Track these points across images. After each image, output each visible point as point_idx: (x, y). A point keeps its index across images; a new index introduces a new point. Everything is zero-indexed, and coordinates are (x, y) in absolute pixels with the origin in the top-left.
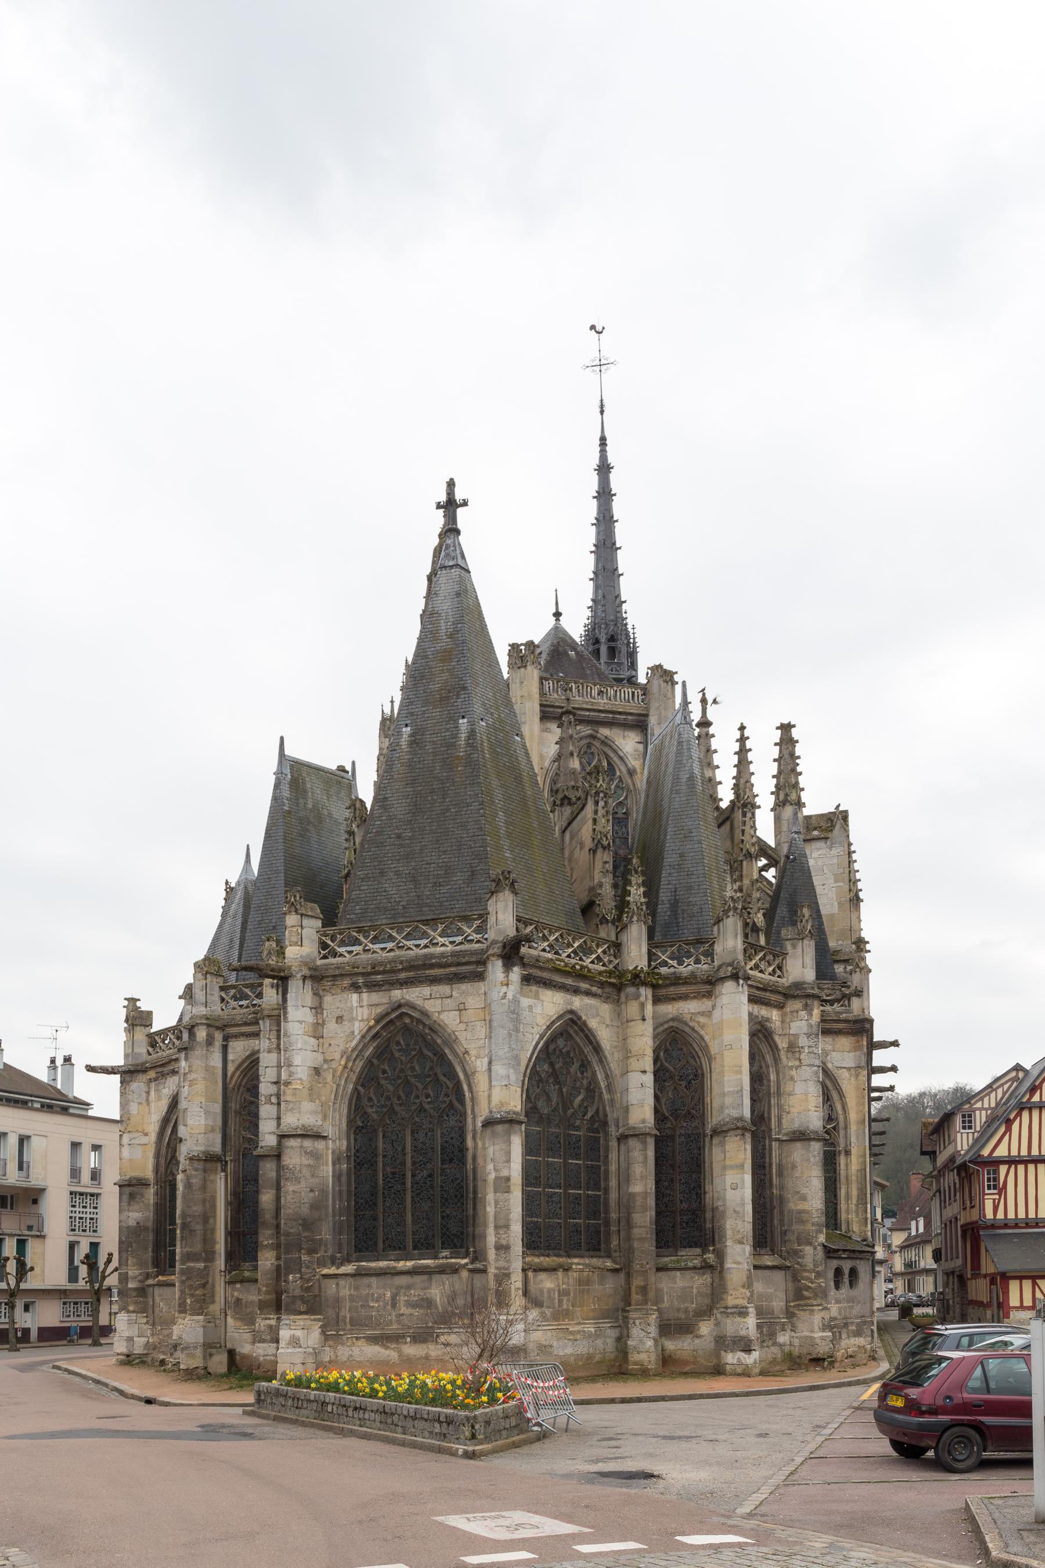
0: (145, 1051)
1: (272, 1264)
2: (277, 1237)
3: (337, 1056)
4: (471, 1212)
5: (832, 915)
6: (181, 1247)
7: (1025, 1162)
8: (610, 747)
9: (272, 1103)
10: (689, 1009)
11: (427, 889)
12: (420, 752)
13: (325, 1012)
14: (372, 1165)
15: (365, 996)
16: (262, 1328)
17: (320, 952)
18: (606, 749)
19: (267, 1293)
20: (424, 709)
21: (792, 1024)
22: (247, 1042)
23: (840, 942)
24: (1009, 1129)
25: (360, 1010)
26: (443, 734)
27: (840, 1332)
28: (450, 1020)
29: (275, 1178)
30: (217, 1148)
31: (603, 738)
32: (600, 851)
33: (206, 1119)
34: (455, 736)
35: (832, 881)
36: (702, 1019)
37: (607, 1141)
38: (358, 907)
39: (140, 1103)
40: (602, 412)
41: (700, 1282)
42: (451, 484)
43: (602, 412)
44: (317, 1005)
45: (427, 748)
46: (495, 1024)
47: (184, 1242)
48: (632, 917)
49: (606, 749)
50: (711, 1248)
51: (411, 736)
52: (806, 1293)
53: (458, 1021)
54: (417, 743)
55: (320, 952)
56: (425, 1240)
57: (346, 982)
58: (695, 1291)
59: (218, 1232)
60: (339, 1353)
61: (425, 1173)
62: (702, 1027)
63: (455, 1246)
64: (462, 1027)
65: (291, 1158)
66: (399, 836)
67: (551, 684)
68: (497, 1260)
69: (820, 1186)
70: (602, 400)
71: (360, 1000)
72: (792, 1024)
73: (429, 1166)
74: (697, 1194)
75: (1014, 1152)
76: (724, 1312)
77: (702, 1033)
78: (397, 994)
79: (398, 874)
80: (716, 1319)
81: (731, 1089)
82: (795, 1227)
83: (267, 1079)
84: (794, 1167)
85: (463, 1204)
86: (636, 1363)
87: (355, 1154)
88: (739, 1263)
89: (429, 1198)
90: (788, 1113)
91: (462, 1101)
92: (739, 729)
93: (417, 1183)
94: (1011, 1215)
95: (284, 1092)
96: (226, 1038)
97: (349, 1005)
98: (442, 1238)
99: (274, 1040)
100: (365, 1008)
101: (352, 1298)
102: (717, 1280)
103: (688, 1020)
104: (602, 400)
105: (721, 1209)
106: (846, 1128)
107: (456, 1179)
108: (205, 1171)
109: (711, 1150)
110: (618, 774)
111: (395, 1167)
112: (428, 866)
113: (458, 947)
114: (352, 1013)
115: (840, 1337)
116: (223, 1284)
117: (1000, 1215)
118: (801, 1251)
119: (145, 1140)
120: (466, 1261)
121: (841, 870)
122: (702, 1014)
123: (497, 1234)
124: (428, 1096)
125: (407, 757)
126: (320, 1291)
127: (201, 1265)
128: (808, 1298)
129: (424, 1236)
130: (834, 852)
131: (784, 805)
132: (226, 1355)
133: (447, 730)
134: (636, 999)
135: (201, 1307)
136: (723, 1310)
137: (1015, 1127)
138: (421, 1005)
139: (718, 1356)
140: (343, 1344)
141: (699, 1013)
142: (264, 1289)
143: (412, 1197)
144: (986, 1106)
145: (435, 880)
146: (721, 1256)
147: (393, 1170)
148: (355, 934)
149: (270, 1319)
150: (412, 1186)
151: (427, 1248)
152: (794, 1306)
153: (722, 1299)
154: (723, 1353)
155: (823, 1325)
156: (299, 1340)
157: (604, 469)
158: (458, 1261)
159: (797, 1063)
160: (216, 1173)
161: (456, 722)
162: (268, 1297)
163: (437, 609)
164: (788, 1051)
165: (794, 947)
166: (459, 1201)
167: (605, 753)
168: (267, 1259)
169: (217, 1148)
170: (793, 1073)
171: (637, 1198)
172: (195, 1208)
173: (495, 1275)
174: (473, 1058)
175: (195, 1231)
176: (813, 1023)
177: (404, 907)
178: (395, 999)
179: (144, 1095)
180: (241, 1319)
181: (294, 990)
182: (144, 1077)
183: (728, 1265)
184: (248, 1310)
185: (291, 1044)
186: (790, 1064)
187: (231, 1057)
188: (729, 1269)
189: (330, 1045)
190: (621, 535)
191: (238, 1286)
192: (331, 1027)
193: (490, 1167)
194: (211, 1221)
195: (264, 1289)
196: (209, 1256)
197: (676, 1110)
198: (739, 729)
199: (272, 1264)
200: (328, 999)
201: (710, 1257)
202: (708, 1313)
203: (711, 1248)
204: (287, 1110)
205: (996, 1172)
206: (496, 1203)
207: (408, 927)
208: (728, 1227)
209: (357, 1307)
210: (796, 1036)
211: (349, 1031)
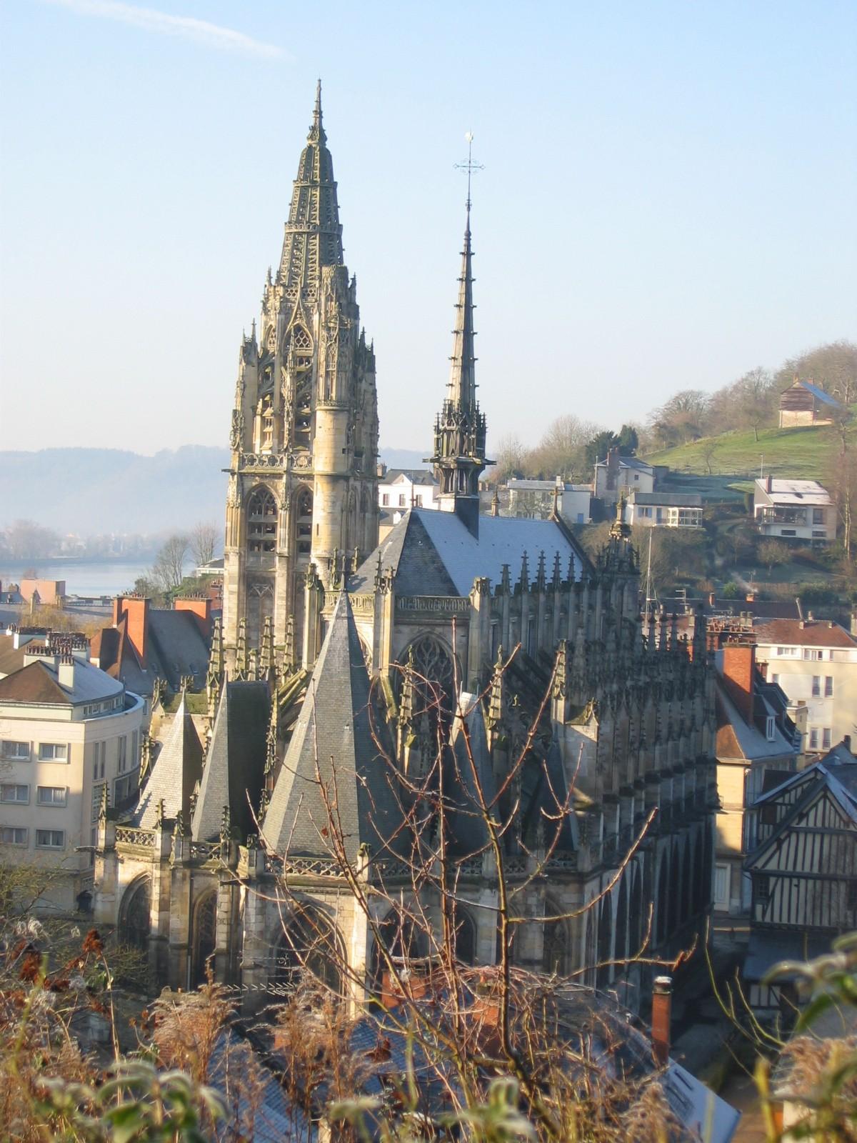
7: (791, 876)
8: (443, 639)
18: (440, 640)
24: (779, 848)
32: (441, 460)
40: (469, 209)
43: (469, 209)
49: (440, 640)
75: (782, 868)
94: (776, 920)
106: (569, 940)
117: (768, 919)
119: (112, 898)
137: (785, 846)
144: (787, 801)
157: (468, 234)
179: (113, 868)
190: (477, 352)
205: (767, 883)
210: (531, 905)
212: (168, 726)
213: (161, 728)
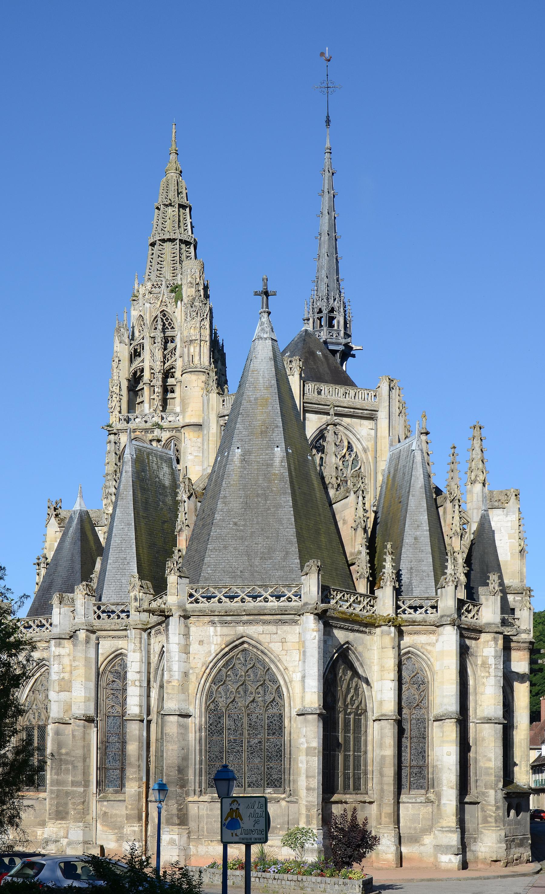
1: (135, 791)
2: (139, 773)
3: (199, 665)
4: (287, 766)
5: (507, 561)
6: (51, 775)
9: (136, 686)
10: (421, 641)
11: (257, 561)
12: (248, 467)
13: (191, 637)
14: (221, 734)
15: (219, 629)
16: (129, 832)
17: (188, 599)
18: (348, 433)
19: (132, 809)
20: (250, 438)
21: (484, 650)
22: (113, 642)
23: (511, 580)
25: (215, 638)
26: (264, 457)
27: (510, 844)
28: (276, 647)
29: (138, 734)
30: (91, 712)
31: (345, 425)
33: (85, 692)
35: (507, 538)
36: (429, 648)
37: (366, 721)
38: (209, 569)
40: (328, 117)
41: (425, 811)
44: (187, 633)
45: (253, 465)
46: (308, 654)
47: (53, 771)
48: (386, 582)
50: (432, 791)
51: (241, 455)
52: (489, 819)
53: (281, 649)
55: (188, 599)
56: (256, 782)
57: (207, 619)
58: (421, 816)
59: (92, 767)
60: (199, 850)
61: (256, 741)
62: (429, 653)
63: (276, 786)
64: (284, 653)
65: (171, 729)
66: (235, 524)
67: (310, 387)
68: (307, 797)
69: (500, 753)
71: (216, 631)
72: (484, 650)
73: (259, 736)
74: (423, 756)
76: (440, 830)
77: (429, 656)
78: (241, 629)
79: (235, 549)
80: (434, 834)
81: (448, 694)
82: (483, 777)
83: (132, 670)
84: (483, 739)
85: (281, 761)
86: (384, 860)
87: (209, 727)
88: (451, 801)
89: (259, 756)
90: (481, 706)
91: (281, 696)
93: (251, 746)
95: (166, 687)
96: (98, 639)
97: (208, 634)
98: (267, 781)
99: (138, 645)
100: (219, 637)
101: (208, 816)
102: (435, 810)
103: (420, 648)
105: (439, 767)
107: (277, 745)
108: (84, 727)
109: (432, 729)
110: (355, 450)
111: (236, 736)
112: (257, 545)
113: (282, 603)
114: (210, 639)
115: (510, 848)
116: (94, 802)
118: (487, 793)
120: (283, 796)
121: (514, 531)
122: (429, 644)
123: (307, 781)
124: (259, 693)
125: (238, 470)
126: (187, 811)
127: (81, 789)
128: (491, 822)
129: (255, 779)
130: (509, 518)
131: (475, 482)
132: (99, 849)
133: (267, 454)
134: (388, 635)
135: (81, 817)
136: (440, 829)
138: (257, 637)
139: (436, 857)
140: (202, 844)
141: (427, 643)
142: (130, 807)
143: (248, 755)
145: (261, 556)
146: (439, 796)
147: (235, 738)
148: (212, 589)
149: (134, 826)
150: (248, 748)
151: (257, 787)
152: (482, 828)
153: (439, 822)
154: (439, 855)
155: (500, 839)
156: (175, 841)
158: (279, 795)
159: (487, 674)
160: (91, 729)
161: (273, 449)
162: (133, 812)
163: (256, 368)
164: (481, 667)
165: (487, 600)
166: (279, 759)
167: (346, 435)
168: (132, 787)
169: (91, 712)
170: (485, 680)
171: (386, 759)
173: (306, 806)
174: (291, 673)
175: (77, 767)
176: (498, 649)
177: (241, 572)
178: (239, 633)
180: (107, 826)
181: (173, 624)
183: (443, 801)
184: (113, 820)
185: (171, 658)
186: (483, 675)
187: (100, 651)
188: (444, 804)
189: (194, 658)
191: (105, 803)
192: (194, 647)
193: (303, 740)
194: (88, 760)
195: (130, 807)
196: (86, 784)
197: (410, 703)
199: (135, 791)
200: (193, 629)
201: (431, 796)
202: (429, 831)
203: (432, 791)
204: (168, 699)
206: (307, 762)
207: (248, 588)
208: (444, 778)
209: (211, 822)
211: (207, 650)
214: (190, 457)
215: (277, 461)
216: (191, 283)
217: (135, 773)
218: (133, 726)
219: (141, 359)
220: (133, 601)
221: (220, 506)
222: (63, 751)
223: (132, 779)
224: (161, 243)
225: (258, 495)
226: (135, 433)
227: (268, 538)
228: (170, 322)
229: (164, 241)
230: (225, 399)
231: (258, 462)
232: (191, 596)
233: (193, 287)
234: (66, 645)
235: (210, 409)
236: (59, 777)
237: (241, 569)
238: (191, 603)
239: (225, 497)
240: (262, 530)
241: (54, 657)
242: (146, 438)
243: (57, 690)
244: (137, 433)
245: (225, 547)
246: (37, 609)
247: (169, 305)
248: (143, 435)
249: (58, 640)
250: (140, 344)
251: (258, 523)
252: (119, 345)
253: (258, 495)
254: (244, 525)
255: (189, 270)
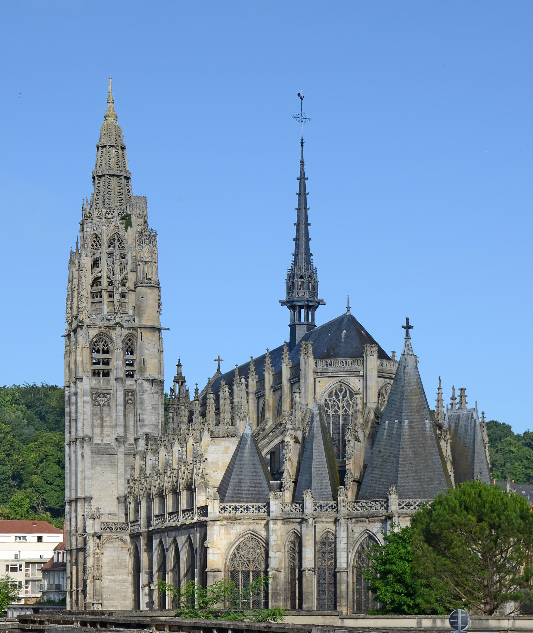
0: (218, 511)
6: (272, 602)
34: (425, 426)
39: (217, 535)
40: (302, 145)
42: (407, 319)
43: (302, 145)
51: (408, 424)
54: (411, 427)
66: (411, 463)
70: (302, 139)
92: (482, 413)
104: (302, 139)
161: (424, 421)
172: (309, 589)
177: (418, 491)
179: (218, 531)
182: (219, 523)
187: (317, 530)
198: (482, 413)
212: (214, 447)
213: (208, 448)
214: (147, 352)
215: (428, 429)
216: (140, 215)
217: (345, 602)
218: (344, 575)
219: (99, 269)
220: (342, 502)
221: (401, 453)
222: (278, 588)
223: (343, 605)
224: (109, 177)
225: (420, 447)
226: (101, 329)
227: (429, 472)
228: (121, 243)
229: (110, 175)
230: (318, 362)
231: (418, 428)
232: (399, 505)
233: (141, 218)
234: (279, 524)
235: (309, 368)
236: (277, 604)
237: (418, 489)
238: (400, 509)
239: (403, 448)
240: (426, 468)
241: (272, 530)
242: (109, 333)
243: (275, 550)
244: (102, 329)
245: (408, 477)
246: (233, 497)
247: (120, 229)
248: (107, 331)
249: (275, 521)
250: (98, 258)
251: (423, 463)
252: (85, 258)
253: (420, 447)
254: (415, 465)
255: (138, 205)
